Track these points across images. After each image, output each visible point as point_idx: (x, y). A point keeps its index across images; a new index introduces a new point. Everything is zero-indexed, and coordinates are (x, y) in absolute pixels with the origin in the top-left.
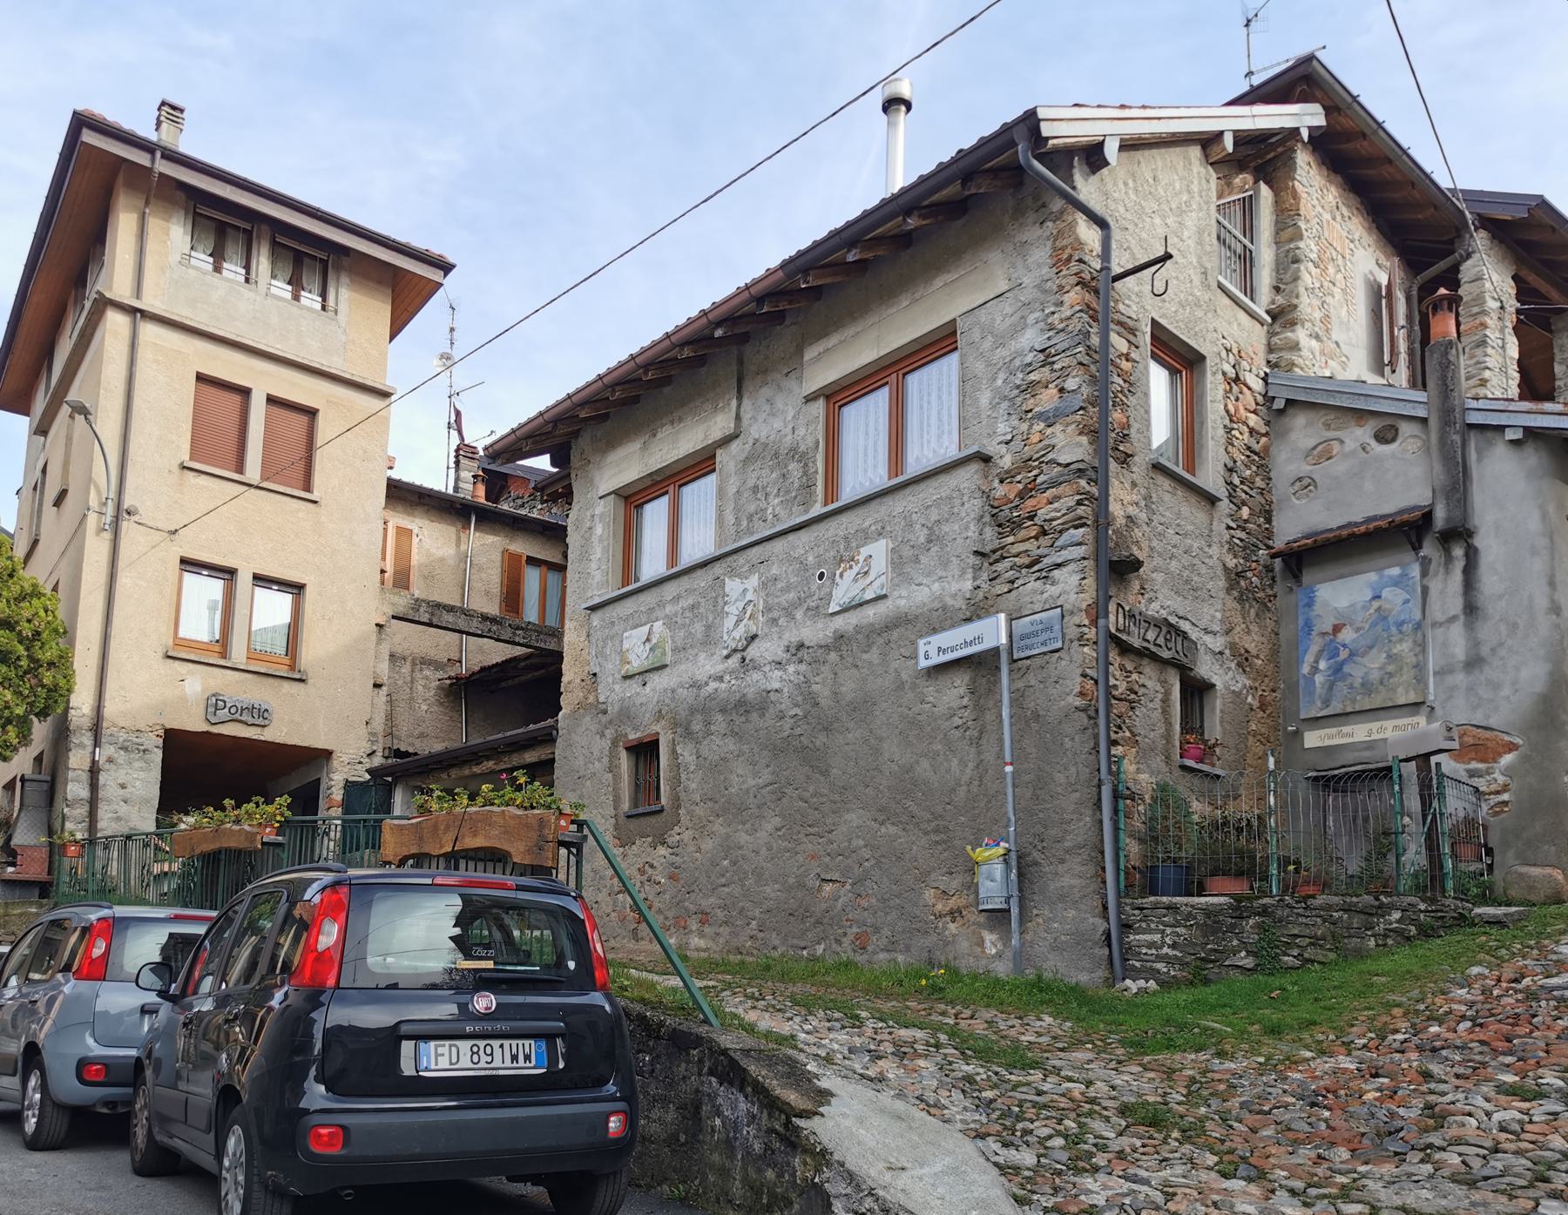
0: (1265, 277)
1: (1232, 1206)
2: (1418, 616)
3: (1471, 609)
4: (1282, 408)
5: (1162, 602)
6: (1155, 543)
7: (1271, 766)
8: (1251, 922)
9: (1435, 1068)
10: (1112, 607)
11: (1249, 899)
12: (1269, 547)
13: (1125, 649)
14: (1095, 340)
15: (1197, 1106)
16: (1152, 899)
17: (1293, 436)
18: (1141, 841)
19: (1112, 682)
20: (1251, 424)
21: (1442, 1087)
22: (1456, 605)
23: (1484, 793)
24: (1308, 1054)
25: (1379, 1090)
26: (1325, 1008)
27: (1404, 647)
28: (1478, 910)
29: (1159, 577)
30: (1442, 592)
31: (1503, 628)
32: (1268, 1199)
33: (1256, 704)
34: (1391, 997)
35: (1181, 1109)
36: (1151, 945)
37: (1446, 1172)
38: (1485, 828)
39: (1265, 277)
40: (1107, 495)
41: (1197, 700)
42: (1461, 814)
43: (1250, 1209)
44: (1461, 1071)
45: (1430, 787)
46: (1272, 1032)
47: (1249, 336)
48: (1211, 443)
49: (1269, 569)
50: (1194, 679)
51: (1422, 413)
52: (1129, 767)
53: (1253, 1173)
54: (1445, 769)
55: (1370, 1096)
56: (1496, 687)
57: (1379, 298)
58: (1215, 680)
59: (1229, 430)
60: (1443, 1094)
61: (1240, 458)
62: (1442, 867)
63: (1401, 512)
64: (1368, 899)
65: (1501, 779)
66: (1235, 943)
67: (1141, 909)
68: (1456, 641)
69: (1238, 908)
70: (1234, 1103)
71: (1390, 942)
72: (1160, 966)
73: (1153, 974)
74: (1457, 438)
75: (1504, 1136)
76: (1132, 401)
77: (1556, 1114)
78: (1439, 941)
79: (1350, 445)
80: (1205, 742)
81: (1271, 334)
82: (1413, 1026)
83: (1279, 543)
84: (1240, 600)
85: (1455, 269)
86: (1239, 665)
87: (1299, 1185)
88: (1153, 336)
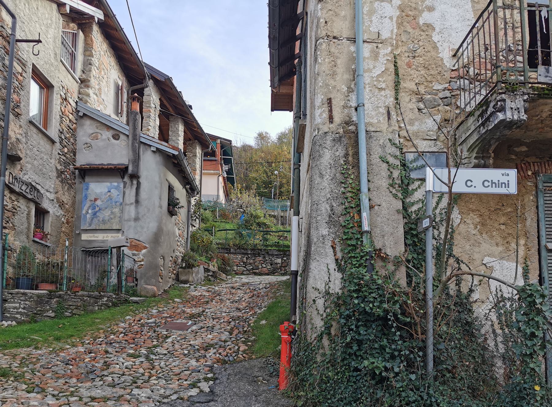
0: (79, 66)
1: (29, 403)
2: (121, 201)
3: (137, 202)
4: (82, 116)
5: (29, 176)
6: (28, 152)
7: (67, 244)
8: (55, 300)
9: (110, 350)
10: (7, 173)
11: (55, 292)
12: (74, 165)
13: (12, 191)
14: (7, 62)
15: (24, 367)
16: (16, 290)
17: (85, 127)
18: (14, 267)
19: (5, 203)
20: (70, 118)
21: (111, 355)
22: (133, 200)
23: (136, 261)
24: (68, 347)
25: (91, 358)
26: (78, 331)
27: (116, 210)
28: (131, 298)
29: (29, 166)
30: (129, 194)
31: (146, 209)
32: (44, 399)
33: (65, 221)
34: (100, 326)
35: (16, 369)
36: (15, 308)
37: (106, 384)
38: (136, 272)
39: (79, 66)
40: (8, 127)
41: (42, 216)
42: (129, 267)
43: (36, 403)
44: (117, 350)
45: (120, 257)
46: (57, 339)
47: (73, 87)
48: (54, 120)
49: (74, 173)
50: (41, 208)
51: (127, 133)
52: (10, 238)
53: (40, 390)
54: (125, 252)
55: (87, 360)
56: (142, 228)
57: (118, 90)
58: (49, 210)
59: (62, 118)
60: (110, 358)
61: (65, 129)
62: (121, 284)
63: (119, 165)
64: (97, 293)
65: (142, 257)
66: (48, 307)
67: (12, 294)
68: (131, 211)
69: (50, 295)
70: (38, 365)
71: (103, 308)
72: (18, 316)
73: (15, 319)
74: (137, 145)
75: (126, 370)
76: (22, 93)
77: (142, 362)
78: (118, 308)
79: (104, 137)
80: (44, 233)
81: (80, 87)
82: (106, 336)
83: (78, 165)
84: (62, 182)
85: (143, 89)
86: (59, 206)
87: (56, 393)
88: (33, 70)
